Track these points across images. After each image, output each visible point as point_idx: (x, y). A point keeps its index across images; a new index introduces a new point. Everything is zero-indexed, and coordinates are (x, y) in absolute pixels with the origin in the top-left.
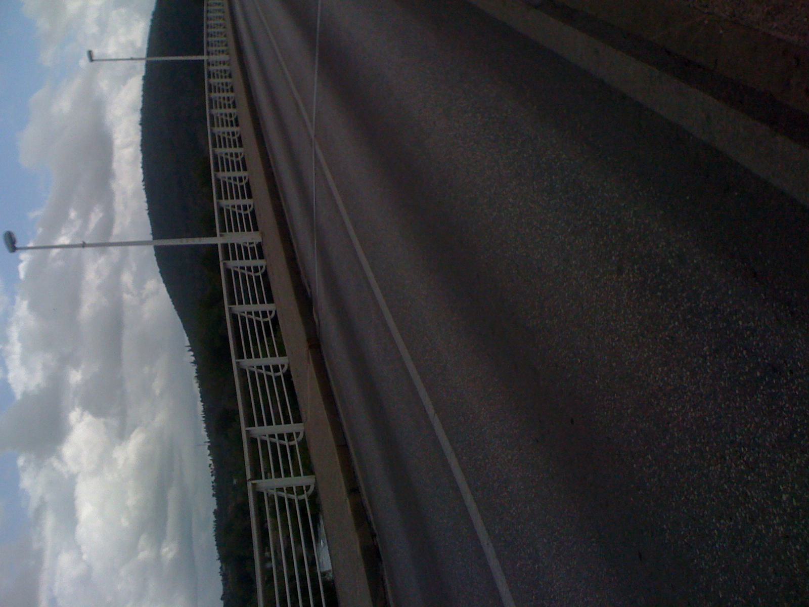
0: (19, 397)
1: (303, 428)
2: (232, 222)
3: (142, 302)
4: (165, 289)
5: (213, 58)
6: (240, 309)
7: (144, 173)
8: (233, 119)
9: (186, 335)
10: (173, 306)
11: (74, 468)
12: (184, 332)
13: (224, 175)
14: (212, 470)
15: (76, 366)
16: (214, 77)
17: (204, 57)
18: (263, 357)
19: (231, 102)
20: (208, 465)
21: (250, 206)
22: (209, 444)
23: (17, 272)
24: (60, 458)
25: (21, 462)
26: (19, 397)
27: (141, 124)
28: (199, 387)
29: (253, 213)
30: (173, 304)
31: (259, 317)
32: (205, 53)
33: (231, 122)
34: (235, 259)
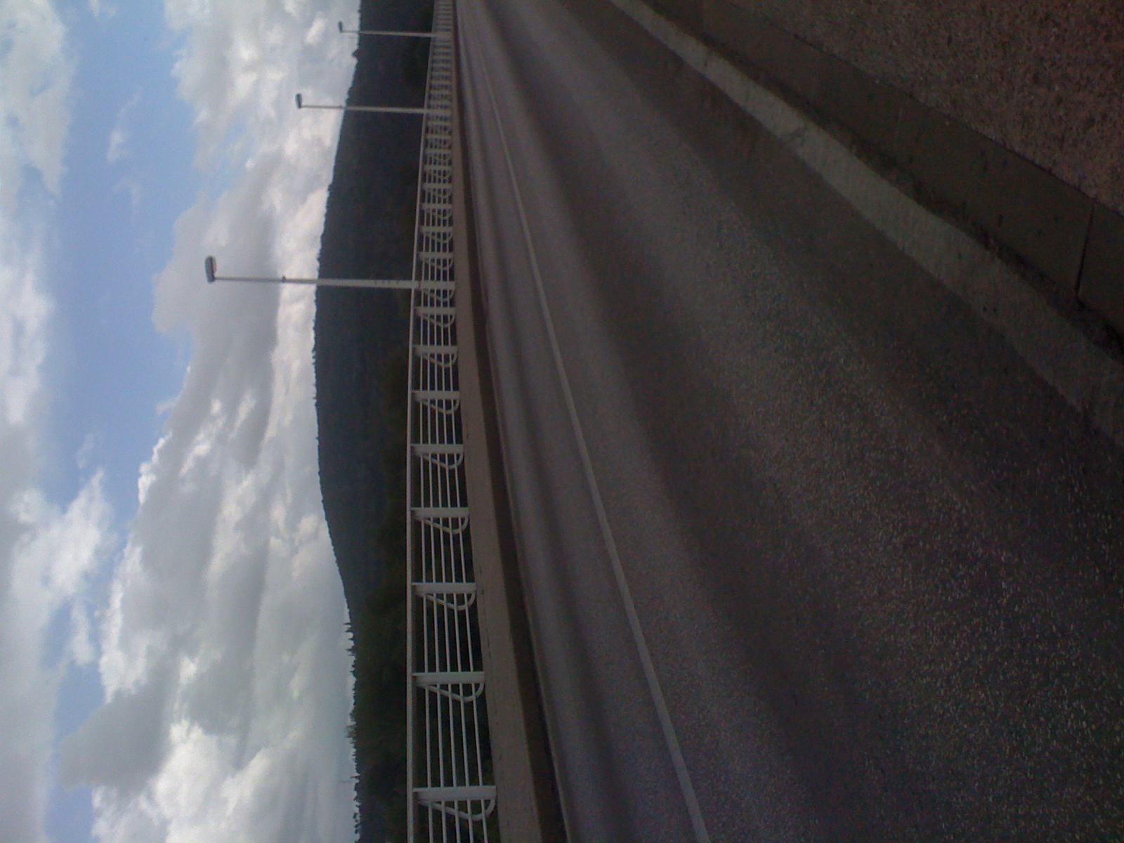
0: (109, 699)
1: (494, 795)
2: (425, 272)
3: (295, 551)
4: (327, 530)
5: (432, 112)
6: (427, 513)
7: (316, 377)
8: (447, 241)
9: (346, 605)
10: (334, 558)
11: (168, 812)
12: (345, 600)
13: (426, 449)
14: (356, 823)
15: (192, 653)
16: (431, 147)
17: (424, 111)
18: (452, 506)
19: (447, 196)
20: (353, 815)
21: (458, 456)
22: (358, 781)
23: (136, 490)
24: (150, 797)
25: (97, 800)
26: (109, 699)
27: (319, 259)
28: (353, 666)
29: (458, 413)
30: (335, 554)
31: (453, 603)
32: (425, 106)
33: (444, 221)
34: (432, 669)
